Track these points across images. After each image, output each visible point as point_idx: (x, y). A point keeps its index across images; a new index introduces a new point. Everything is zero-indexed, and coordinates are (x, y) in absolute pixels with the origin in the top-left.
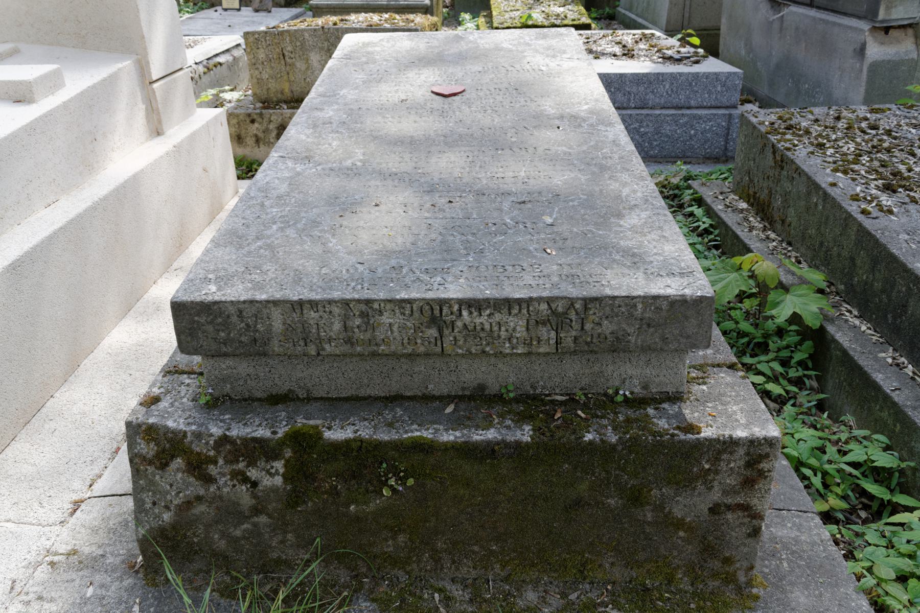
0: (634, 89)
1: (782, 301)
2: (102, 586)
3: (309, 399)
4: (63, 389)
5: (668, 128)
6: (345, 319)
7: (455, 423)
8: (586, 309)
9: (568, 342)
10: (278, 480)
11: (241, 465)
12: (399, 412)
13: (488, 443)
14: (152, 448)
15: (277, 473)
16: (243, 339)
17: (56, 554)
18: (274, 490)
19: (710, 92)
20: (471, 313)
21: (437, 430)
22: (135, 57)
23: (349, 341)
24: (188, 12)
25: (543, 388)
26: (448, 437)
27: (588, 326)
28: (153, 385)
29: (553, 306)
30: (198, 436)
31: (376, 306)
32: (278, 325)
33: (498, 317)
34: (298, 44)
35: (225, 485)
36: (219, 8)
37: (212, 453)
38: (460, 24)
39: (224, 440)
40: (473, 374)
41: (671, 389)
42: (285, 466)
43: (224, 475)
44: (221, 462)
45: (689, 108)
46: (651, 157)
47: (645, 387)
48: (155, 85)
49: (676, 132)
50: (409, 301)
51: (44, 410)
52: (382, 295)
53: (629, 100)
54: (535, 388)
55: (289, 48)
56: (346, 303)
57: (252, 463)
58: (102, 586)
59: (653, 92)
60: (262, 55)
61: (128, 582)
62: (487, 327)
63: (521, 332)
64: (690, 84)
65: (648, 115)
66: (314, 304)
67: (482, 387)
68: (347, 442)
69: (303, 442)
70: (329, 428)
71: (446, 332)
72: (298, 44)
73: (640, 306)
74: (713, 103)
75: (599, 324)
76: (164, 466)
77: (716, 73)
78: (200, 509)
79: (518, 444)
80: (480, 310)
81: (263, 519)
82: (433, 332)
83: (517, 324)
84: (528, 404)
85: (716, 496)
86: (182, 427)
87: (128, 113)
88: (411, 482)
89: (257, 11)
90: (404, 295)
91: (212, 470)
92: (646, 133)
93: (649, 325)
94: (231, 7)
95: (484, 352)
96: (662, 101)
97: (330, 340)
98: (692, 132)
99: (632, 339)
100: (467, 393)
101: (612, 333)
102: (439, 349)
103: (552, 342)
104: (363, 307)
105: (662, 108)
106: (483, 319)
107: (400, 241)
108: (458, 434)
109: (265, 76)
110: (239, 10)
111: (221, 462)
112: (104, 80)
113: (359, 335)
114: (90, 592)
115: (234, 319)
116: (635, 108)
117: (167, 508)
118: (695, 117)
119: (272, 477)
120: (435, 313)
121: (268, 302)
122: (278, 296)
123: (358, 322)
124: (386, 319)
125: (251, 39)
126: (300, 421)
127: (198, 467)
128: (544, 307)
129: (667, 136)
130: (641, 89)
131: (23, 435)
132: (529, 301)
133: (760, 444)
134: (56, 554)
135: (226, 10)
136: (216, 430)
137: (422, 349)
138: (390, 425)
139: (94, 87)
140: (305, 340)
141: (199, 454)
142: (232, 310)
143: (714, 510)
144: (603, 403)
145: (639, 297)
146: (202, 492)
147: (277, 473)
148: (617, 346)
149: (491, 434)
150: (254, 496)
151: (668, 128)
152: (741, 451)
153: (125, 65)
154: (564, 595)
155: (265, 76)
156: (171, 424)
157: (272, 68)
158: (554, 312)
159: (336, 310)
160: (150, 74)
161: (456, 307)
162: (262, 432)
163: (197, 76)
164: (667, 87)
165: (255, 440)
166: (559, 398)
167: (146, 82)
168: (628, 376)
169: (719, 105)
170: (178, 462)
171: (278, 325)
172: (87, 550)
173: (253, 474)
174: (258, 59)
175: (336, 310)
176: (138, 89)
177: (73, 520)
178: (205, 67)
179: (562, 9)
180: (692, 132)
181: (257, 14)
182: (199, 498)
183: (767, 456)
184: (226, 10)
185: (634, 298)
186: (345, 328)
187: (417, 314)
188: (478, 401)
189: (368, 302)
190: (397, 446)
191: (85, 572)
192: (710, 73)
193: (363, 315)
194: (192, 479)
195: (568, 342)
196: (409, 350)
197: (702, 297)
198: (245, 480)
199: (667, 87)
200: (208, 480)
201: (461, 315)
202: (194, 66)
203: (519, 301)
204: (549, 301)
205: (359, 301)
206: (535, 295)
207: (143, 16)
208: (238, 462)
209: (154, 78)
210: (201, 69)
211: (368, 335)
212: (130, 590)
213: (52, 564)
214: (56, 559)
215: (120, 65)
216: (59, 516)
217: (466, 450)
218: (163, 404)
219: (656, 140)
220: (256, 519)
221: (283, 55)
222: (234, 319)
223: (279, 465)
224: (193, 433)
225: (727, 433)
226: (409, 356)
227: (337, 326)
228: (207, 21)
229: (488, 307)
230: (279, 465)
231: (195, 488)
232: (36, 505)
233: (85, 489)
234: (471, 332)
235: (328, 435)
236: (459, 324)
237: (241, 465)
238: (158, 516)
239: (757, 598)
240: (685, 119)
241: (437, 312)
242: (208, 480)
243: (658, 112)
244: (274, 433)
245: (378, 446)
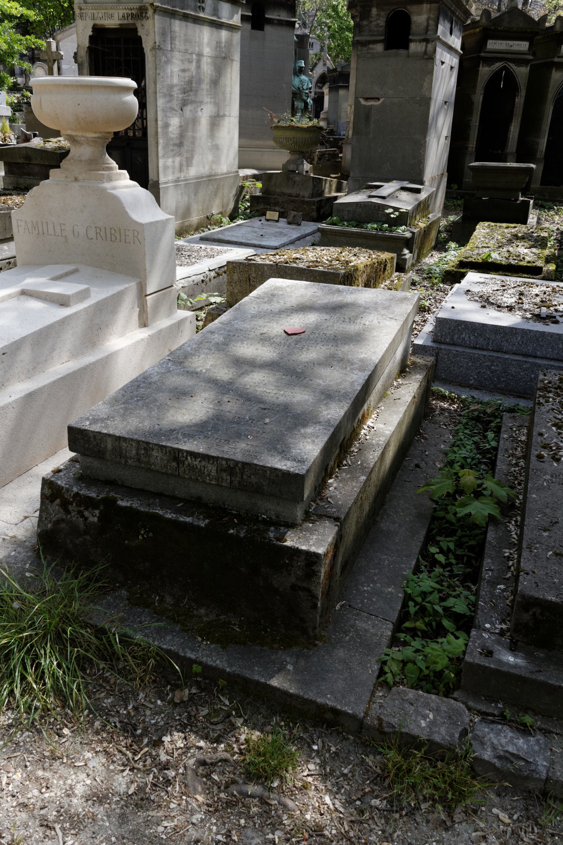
0: (493, 337)
1: (469, 504)
2: (19, 553)
3: (123, 486)
4: (44, 463)
5: (514, 369)
6: (138, 449)
7: (178, 511)
8: (244, 468)
9: (236, 483)
10: (96, 519)
11: (82, 508)
12: (157, 500)
13: (185, 523)
14: (51, 490)
15: (96, 516)
16: (95, 449)
17: (7, 536)
18: (93, 523)
19: (553, 348)
20: (191, 459)
21: (167, 512)
22: (139, 280)
23: (139, 460)
24: (241, 219)
25: (228, 505)
26: (169, 516)
27: (245, 477)
28: (62, 465)
29: (229, 463)
30: (68, 490)
31: (151, 446)
32: (109, 446)
33: (203, 463)
34: (260, 273)
35: (74, 517)
36: (263, 218)
37: (71, 500)
38: (446, 251)
39: (77, 494)
40: (196, 490)
41: (290, 521)
42: (99, 513)
43: (74, 511)
44: (74, 505)
45: (535, 357)
46: (499, 389)
47: (278, 516)
48: (148, 297)
49: (519, 373)
50: (165, 447)
51: (30, 471)
52: (155, 442)
53: (488, 344)
54: (224, 505)
55: (254, 275)
56: (138, 442)
57: (86, 509)
58: (19, 553)
59: (507, 341)
60: (236, 277)
61: (30, 554)
62: (199, 467)
63: (214, 473)
64: (538, 340)
65: (498, 357)
66: (125, 439)
67: (199, 498)
68: (126, 507)
69: (109, 503)
70: (122, 500)
71: (181, 465)
72: (260, 273)
73: (268, 472)
74: (555, 357)
75: (250, 477)
76: (52, 502)
77: (558, 334)
78: (63, 525)
79: (198, 526)
80: (195, 458)
81: (88, 537)
82: (174, 464)
83: (212, 469)
84: (216, 511)
85: (293, 580)
86: (63, 485)
87: (128, 311)
88: (151, 534)
89: (289, 223)
90: (164, 444)
91: (70, 508)
92: (496, 371)
93: (273, 483)
94: (272, 218)
95: (197, 479)
96: (514, 348)
97: (131, 458)
98: (533, 376)
99: (266, 488)
100: (193, 499)
101: (256, 483)
102: (177, 473)
103: (228, 481)
104: (145, 445)
105: (513, 354)
106: (197, 463)
107: (204, 418)
108: (174, 516)
109: (236, 291)
110: (277, 221)
111: (74, 505)
112: (114, 295)
113: (143, 458)
114: (13, 553)
115: (92, 439)
116: (492, 350)
117: (50, 521)
118: (535, 365)
119: (93, 517)
120: (177, 456)
121: (106, 434)
122: (111, 432)
123: (143, 452)
124: (155, 453)
125: (231, 266)
126: (112, 494)
127: (65, 505)
128: (224, 462)
129: (512, 375)
130: (498, 337)
131: (16, 481)
132: (217, 458)
133: (311, 555)
134: (7, 536)
135: (268, 220)
136: (75, 489)
137: (170, 472)
138: (149, 505)
139: (106, 299)
140: (120, 455)
141: (66, 499)
142: (91, 435)
143: (293, 587)
144: (249, 518)
145: (268, 467)
146: (64, 517)
147: (96, 516)
148: (258, 490)
149: (189, 519)
150: (85, 525)
151: (514, 369)
152: (303, 557)
153: (131, 286)
154: (217, 615)
155: (236, 291)
156: (59, 482)
157: (241, 286)
158: (229, 466)
159: (134, 444)
160: (146, 290)
161: (185, 454)
162: (93, 495)
163: (208, 279)
164: (519, 339)
165: (88, 497)
166: (234, 512)
167: (142, 295)
168: (269, 508)
169: (560, 358)
170: (58, 501)
171: (109, 446)
172: (20, 537)
173: (86, 514)
174: (233, 279)
175: (134, 444)
176: (136, 300)
177: (20, 524)
178: (216, 273)
179: (526, 251)
180: (533, 376)
181: (289, 226)
182: (63, 520)
183: (316, 563)
184: (268, 220)
185: (265, 467)
186: (137, 454)
187: (168, 454)
188: (195, 504)
189: (148, 443)
190: (147, 514)
191: (15, 546)
192: (554, 334)
193: (145, 449)
194: (62, 510)
195: (236, 483)
196: (164, 470)
197: (297, 474)
198: (83, 516)
199: (519, 339)
200: (68, 512)
201: (187, 458)
202: (208, 273)
203: (213, 457)
204: (227, 460)
205: (143, 442)
206: (220, 456)
207: (147, 257)
208: (81, 506)
209: (148, 293)
210: (213, 274)
211: (146, 460)
212: (29, 557)
213: (4, 539)
214: (6, 537)
215: (127, 286)
216: (16, 521)
217: (175, 523)
218: (62, 474)
219: (503, 377)
220: (85, 537)
221: (249, 279)
222: (92, 439)
223: (97, 512)
224: (66, 488)
225: (297, 546)
226: (163, 474)
227: (134, 452)
228: (249, 229)
229: (199, 457)
230: (97, 512)
231: (62, 515)
232: (9, 514)
233: (32, 512)
234: (192, 468)
235: (120, 503)
236: (186, 463)
237: (82, 508)
238: (46, 525)
239: (316, 645)
240: (528, 365)
241: (177, 455)
242: (68, 512)
243: (507, 356)
244: (98, 496)
245: (138, 512)
